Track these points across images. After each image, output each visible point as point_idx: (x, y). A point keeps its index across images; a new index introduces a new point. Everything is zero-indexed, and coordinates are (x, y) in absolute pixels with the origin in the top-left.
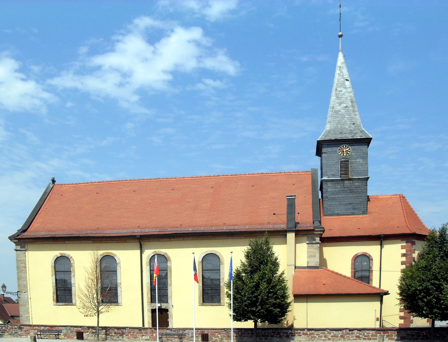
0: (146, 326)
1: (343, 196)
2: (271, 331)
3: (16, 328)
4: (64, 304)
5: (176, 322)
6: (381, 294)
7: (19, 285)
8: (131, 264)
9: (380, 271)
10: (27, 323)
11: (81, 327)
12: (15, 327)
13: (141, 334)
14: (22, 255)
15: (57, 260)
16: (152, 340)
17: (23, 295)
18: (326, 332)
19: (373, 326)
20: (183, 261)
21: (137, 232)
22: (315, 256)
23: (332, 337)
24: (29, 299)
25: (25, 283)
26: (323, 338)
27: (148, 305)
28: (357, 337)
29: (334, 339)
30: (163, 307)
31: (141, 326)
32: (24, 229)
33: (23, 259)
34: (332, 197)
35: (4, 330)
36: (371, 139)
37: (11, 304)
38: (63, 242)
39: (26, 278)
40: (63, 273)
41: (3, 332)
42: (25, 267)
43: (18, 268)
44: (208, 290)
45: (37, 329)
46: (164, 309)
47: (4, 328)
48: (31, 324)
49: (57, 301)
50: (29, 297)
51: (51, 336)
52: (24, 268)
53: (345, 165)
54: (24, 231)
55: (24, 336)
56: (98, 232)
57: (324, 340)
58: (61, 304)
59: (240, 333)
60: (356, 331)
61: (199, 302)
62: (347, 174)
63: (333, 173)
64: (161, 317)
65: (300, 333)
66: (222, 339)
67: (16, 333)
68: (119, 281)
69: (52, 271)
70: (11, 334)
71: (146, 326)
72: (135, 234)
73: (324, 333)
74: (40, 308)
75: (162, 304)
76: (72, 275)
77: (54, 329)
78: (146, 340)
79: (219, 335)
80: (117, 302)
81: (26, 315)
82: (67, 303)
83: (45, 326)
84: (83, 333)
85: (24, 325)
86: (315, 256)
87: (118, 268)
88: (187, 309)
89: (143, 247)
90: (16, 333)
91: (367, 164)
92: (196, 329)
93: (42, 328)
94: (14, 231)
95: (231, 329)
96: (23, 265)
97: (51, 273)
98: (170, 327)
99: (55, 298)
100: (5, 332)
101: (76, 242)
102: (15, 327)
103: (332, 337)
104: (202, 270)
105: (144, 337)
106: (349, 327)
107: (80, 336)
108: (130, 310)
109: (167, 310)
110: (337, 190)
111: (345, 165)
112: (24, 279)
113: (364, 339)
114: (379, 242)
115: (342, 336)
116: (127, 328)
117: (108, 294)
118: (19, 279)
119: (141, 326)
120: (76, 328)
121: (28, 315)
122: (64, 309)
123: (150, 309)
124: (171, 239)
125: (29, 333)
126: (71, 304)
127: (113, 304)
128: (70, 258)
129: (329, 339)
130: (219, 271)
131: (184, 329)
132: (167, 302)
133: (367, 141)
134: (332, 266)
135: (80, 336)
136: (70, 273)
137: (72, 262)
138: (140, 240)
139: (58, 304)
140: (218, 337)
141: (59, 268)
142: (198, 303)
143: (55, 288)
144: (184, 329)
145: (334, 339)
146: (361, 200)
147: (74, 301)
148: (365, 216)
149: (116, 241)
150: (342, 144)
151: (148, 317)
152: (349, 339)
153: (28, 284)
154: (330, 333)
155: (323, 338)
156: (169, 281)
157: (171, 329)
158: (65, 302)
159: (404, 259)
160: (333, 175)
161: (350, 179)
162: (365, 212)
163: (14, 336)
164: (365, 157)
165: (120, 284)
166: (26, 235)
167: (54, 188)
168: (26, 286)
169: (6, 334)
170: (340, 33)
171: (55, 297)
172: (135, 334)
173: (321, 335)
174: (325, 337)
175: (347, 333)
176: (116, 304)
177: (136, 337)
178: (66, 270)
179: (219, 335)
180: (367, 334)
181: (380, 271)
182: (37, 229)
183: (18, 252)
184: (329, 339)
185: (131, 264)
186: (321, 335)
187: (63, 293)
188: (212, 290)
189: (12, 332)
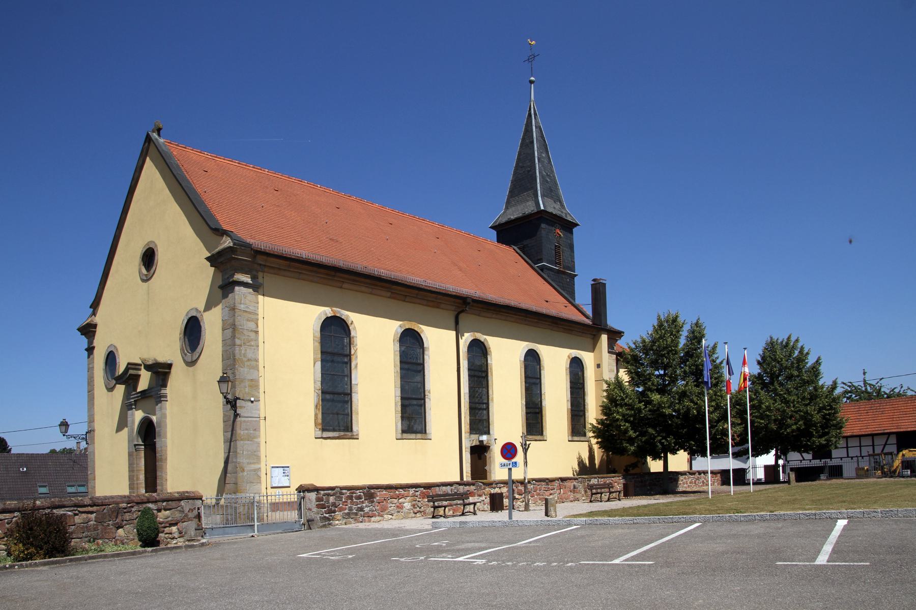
3: (359, 497)
24: (262, 422)
31: (458, 479)
35: (334, 505)
39: (257, 360)
41: (330, 512)
42: (257, 332)
50: (262, 416)
52: (252, 335)
55: (378, 518)
81: (253, 467)
82: (342, 433)
92: (712, 472)
95: (729, 471)
100: (334, 512)
101: (363, 289)
112: (254, 363)
117: (413, 416)
119: (458, 479)
121: (256, 466)
122: (336, 447)
123: (469, 446)
126: (349, 434)
130: (474, 406)
139: (326, 434)
147: (355, 429)
148: (865, 481)
153: (261, 380)
169: (338, 515)
170: (532, 78)
187: (336, 412)
189: (350, 509)
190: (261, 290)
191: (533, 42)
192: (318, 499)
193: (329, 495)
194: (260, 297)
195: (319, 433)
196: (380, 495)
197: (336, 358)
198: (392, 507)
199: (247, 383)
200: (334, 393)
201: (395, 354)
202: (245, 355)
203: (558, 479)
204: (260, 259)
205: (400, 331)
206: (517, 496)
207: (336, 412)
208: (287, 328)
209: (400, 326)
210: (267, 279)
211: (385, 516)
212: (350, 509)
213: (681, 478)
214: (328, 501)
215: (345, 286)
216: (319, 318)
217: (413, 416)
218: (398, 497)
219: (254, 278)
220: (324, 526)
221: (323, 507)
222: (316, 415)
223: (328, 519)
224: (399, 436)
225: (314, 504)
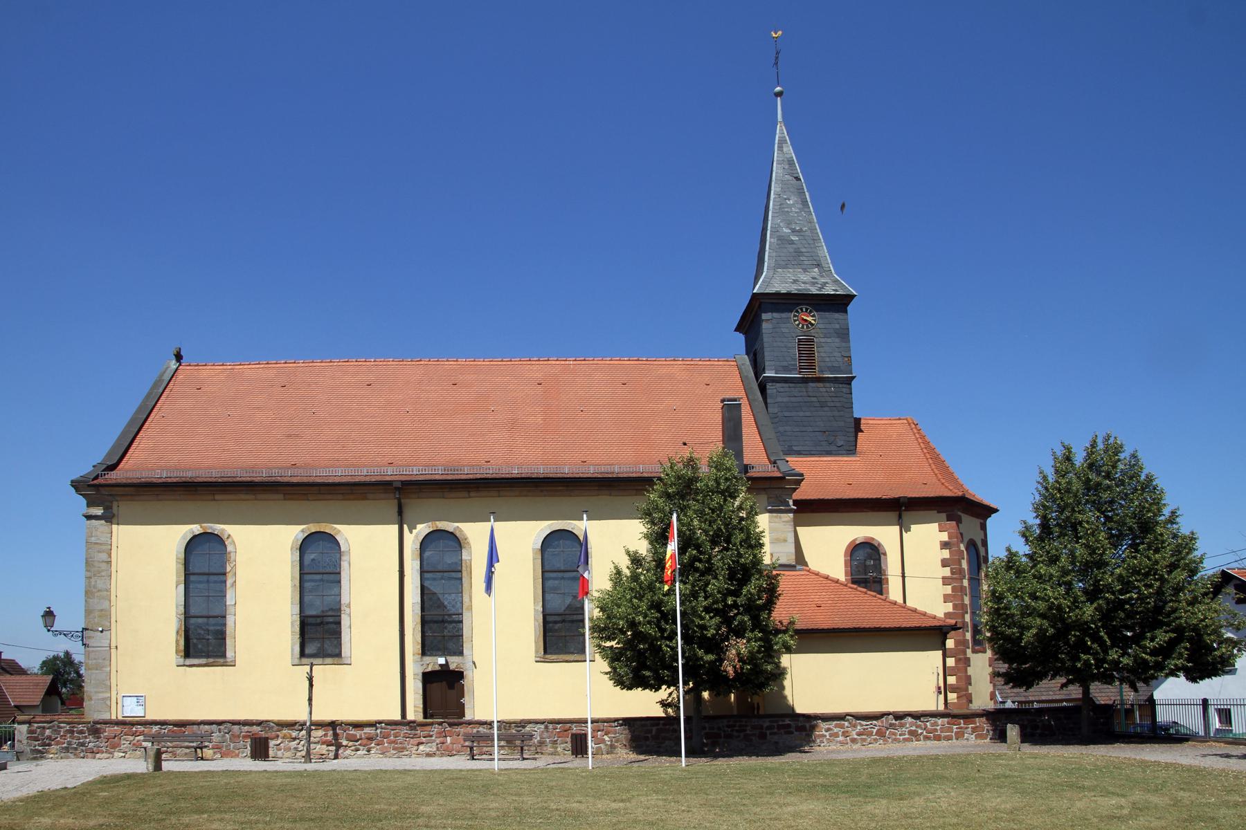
0: (411, 716)
1: (808, 414)
2: (725, 722)
3: (81, 732)
4: (203, 661)
5: (487, 700)
6: (945, 630)
7: (88, 612)
8: (375, 558)
9: (903, 577)
10: (106, 716)
11: (259, 723)
12: (80, 727)
13: (416, 741)
14: (102, 529)
15: (192, 545)
16: (442, 755)
17: (96, 640)
18: (846, 724)
19: (931, 707)
20: (508, 548)
21: (391, 473)
22: (785, 541)
23: (859, 734)
24: (113, 651)
25: (105, 605)
26: (841, 738)
27: (415, 661)
28: (912, 733)
29: (864, 740)
30: (452, 667)
31: (398, 717)
32: (110, 463)
33: (103, 540)
34: (787, 414)
35: (49, 738)
36: (852, 297)
37: (18, 677)
38: (211, 497)
39: (109, 590)
40: (205, 578)
41: (44, 745)
43: (89, 563)
44: (556, 622)
45: (142, 733)
46: (453, 671)
47: (48, 732)
48: (114, 717)
49: (187, 654)
50: (113, 645)
51: (179, 751)
52: (104, 566)
53: (806, 348)
54: (112, 468)
55: (105, 755)
56: (296, 472)
57: (842, 743)
58: (196, 661)
59: (654, 729)
60: (910, 719)
61: (537, 652)
62: (811, 366)
63: (785, 364)
64: (444, 691)
65: (789, 726)
66: (612, 747)
67: (83, 744)
68: (344, 600)
69: (177, 573)
70: (67, 749)
71: (411, 716)
72: (388, 478)
73: (842, 727)
74: (144, 675)
75: (449, 659)
76: (229, 582)
77: (188, 731)
78: (428, 755)
79: (606, 738)
80: (339, 655)
81: (102, 695)
82: (211, 660)
83: (163, 723)
84: (267, 739)
85: (106, 722)
86: (785, 541)
87: (344, 564)
88: (510, 674)
89: (408, 513)
90: (83, 744)
91: (849, 349)
93: (155, 728)
94: (83, 468)
95: (490, 724)
96: (104, 556)
97: (174, 578)
98: (468, 717)
99: (182, 647)
100: (49, 745)
101: (243, 496)
102: (80, 727)
103: (859, 734)
104: (543, 572)
105: (421, 747)
106: (891, 710)
107: (579, 746)
108: (373, 677)
109: (459, 675)
110: (793, 399)
111: (806, 348)
113: (927, 738)
114: (893, 515)
115: (881, 734)
116: (380, 722)
117: (320, 634)
118: (89, 593)
119: (398, 717)
120: (246, 728)
121: (580, 617)
122: (204, 676)
123: (420, 671)
124: (472, 494)
125: (119, 745)
126: (222, 660)
127: (329, 660)
128: (225, 537)
129: (854, 741)
131: (522, 724)
132: (461, 653)
133: (839, 303)
134: (815, 561)
135: (579, 746)
136: (222, 577)
137: (230, 548)
138: (397, 496)
139: (189, 661)
140: (603, 741)
141: (198, 565)
142: (533, 654)
143: (182, 617)
144: (522, 721)
145: (864, 740)
146: (842, 424)
147: (229, 654)
149: (340, 497)
150: (799, 304)
151: (416, 693)
152: (895, 740)
153: (113, 609)
154: (855, 726)
155: (841, 738)
156: (466, 599)
157: (470, 723)
158: (208, 657)
159: (946, 554)
160: (786, 369)
161: (819, 380)
162: (851, 450)
163: (76, 756)
164: (844, 334)
165: (349, 606)
166: (114, 476)
167: (180, 376)
168: (106, 614)
169: (54, 748)
170: (778, 89)
171: (182, 642)
172: (400, 739)
173: (836, 730)
174: (845, 734)
175: (891, 725)
176: (336, 660)
177: (404, 749)
178: (212, 570)
179: (606, 738)
180: (932, 725)
181: (903, 577)
182: (145, 461)
183: (94, 522)
184: (854, 741)
185: (375, 558)
186: (836, 730)
187: (204, 640)
188: (564, 621)
190: (114, 520)
191: (780, 33)
192: (30, 732)
193: (44, 728)
194: (115, 527)
195: (181, 661)
196: (109, 731)
197: (212, 578)
198: (125, 744)
199: (97, 614)
200: (208, 617)
201: (293, 566)
202: (95, 587)
203: (229, 722)
204: (104, 491)
205: (302, 536)
206: (345, 743)
207: (204, 640)
208: (149, 555)
209: (303, 531)
210: (121, 508)
211: (116, 754)
212: (69, 743)
213: (823, 725)
214: (43, 734)
215: (217, 497)
216: (184, 537)
217: (320, 634)
218: (134, 734)
219: (107, 509)
220: (35, 759)
221: (36, 739)
222: (177, 641)
223: (39, 751)
224: (297, 661)
225: (25, 735)
